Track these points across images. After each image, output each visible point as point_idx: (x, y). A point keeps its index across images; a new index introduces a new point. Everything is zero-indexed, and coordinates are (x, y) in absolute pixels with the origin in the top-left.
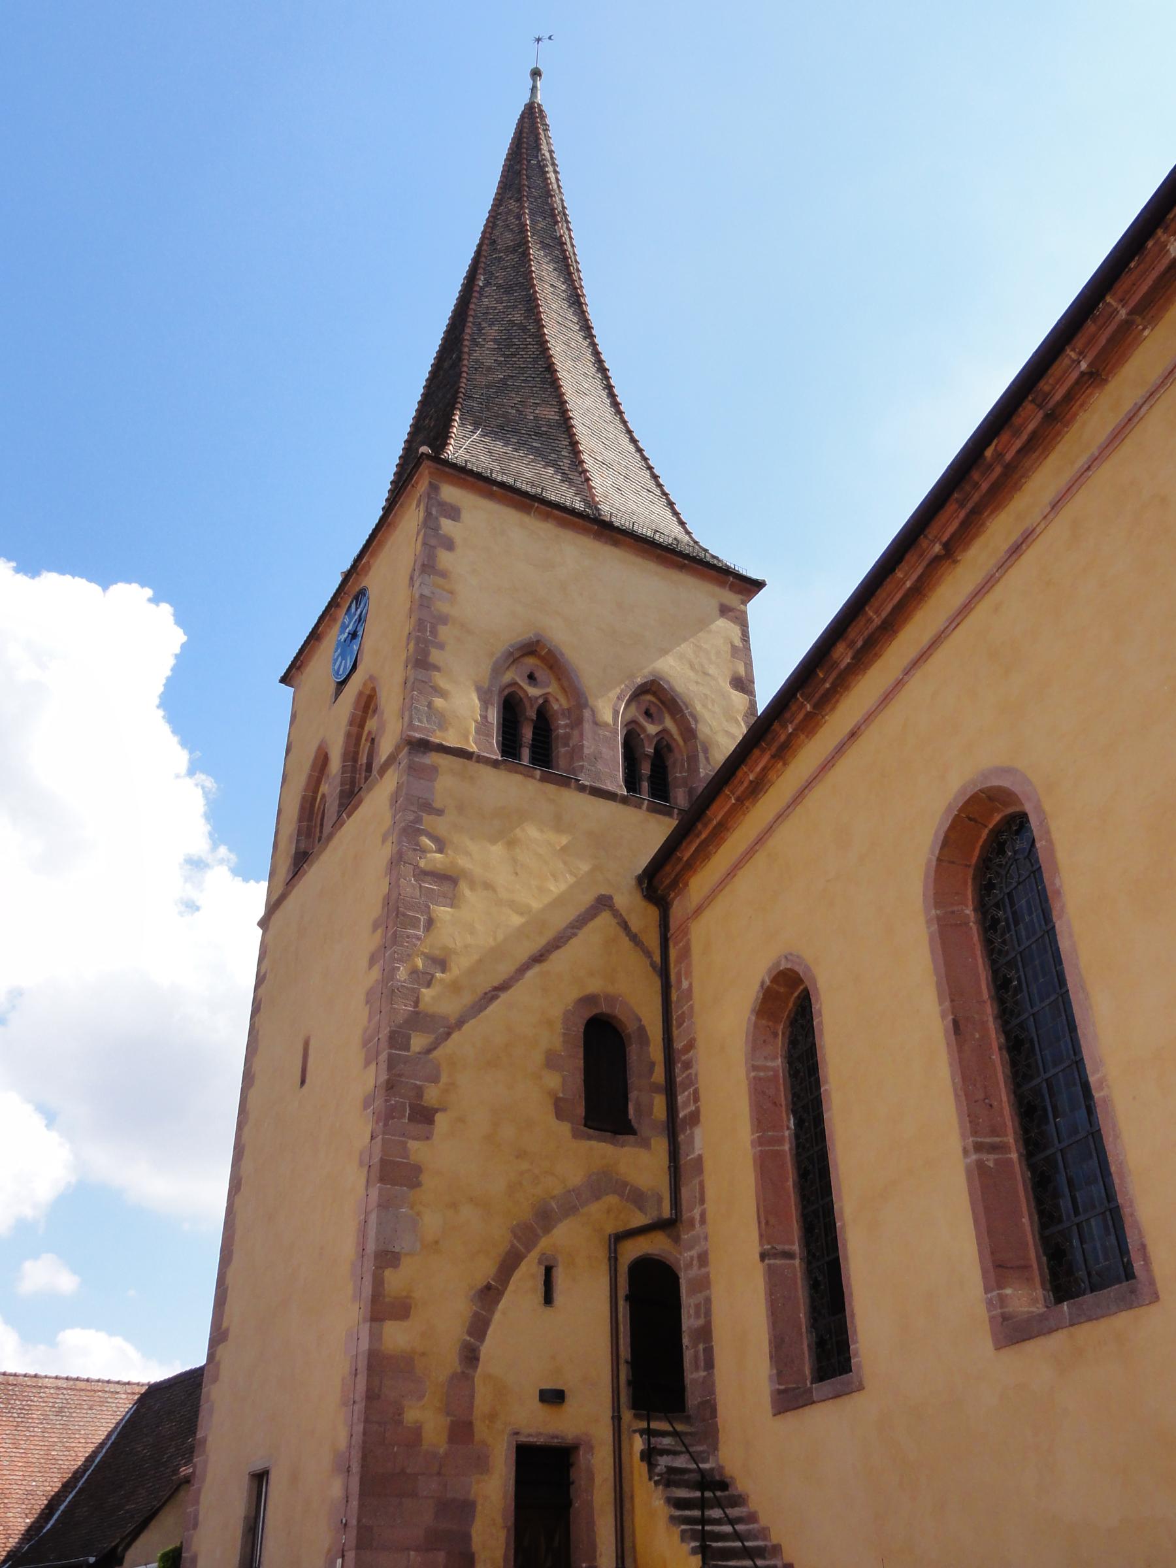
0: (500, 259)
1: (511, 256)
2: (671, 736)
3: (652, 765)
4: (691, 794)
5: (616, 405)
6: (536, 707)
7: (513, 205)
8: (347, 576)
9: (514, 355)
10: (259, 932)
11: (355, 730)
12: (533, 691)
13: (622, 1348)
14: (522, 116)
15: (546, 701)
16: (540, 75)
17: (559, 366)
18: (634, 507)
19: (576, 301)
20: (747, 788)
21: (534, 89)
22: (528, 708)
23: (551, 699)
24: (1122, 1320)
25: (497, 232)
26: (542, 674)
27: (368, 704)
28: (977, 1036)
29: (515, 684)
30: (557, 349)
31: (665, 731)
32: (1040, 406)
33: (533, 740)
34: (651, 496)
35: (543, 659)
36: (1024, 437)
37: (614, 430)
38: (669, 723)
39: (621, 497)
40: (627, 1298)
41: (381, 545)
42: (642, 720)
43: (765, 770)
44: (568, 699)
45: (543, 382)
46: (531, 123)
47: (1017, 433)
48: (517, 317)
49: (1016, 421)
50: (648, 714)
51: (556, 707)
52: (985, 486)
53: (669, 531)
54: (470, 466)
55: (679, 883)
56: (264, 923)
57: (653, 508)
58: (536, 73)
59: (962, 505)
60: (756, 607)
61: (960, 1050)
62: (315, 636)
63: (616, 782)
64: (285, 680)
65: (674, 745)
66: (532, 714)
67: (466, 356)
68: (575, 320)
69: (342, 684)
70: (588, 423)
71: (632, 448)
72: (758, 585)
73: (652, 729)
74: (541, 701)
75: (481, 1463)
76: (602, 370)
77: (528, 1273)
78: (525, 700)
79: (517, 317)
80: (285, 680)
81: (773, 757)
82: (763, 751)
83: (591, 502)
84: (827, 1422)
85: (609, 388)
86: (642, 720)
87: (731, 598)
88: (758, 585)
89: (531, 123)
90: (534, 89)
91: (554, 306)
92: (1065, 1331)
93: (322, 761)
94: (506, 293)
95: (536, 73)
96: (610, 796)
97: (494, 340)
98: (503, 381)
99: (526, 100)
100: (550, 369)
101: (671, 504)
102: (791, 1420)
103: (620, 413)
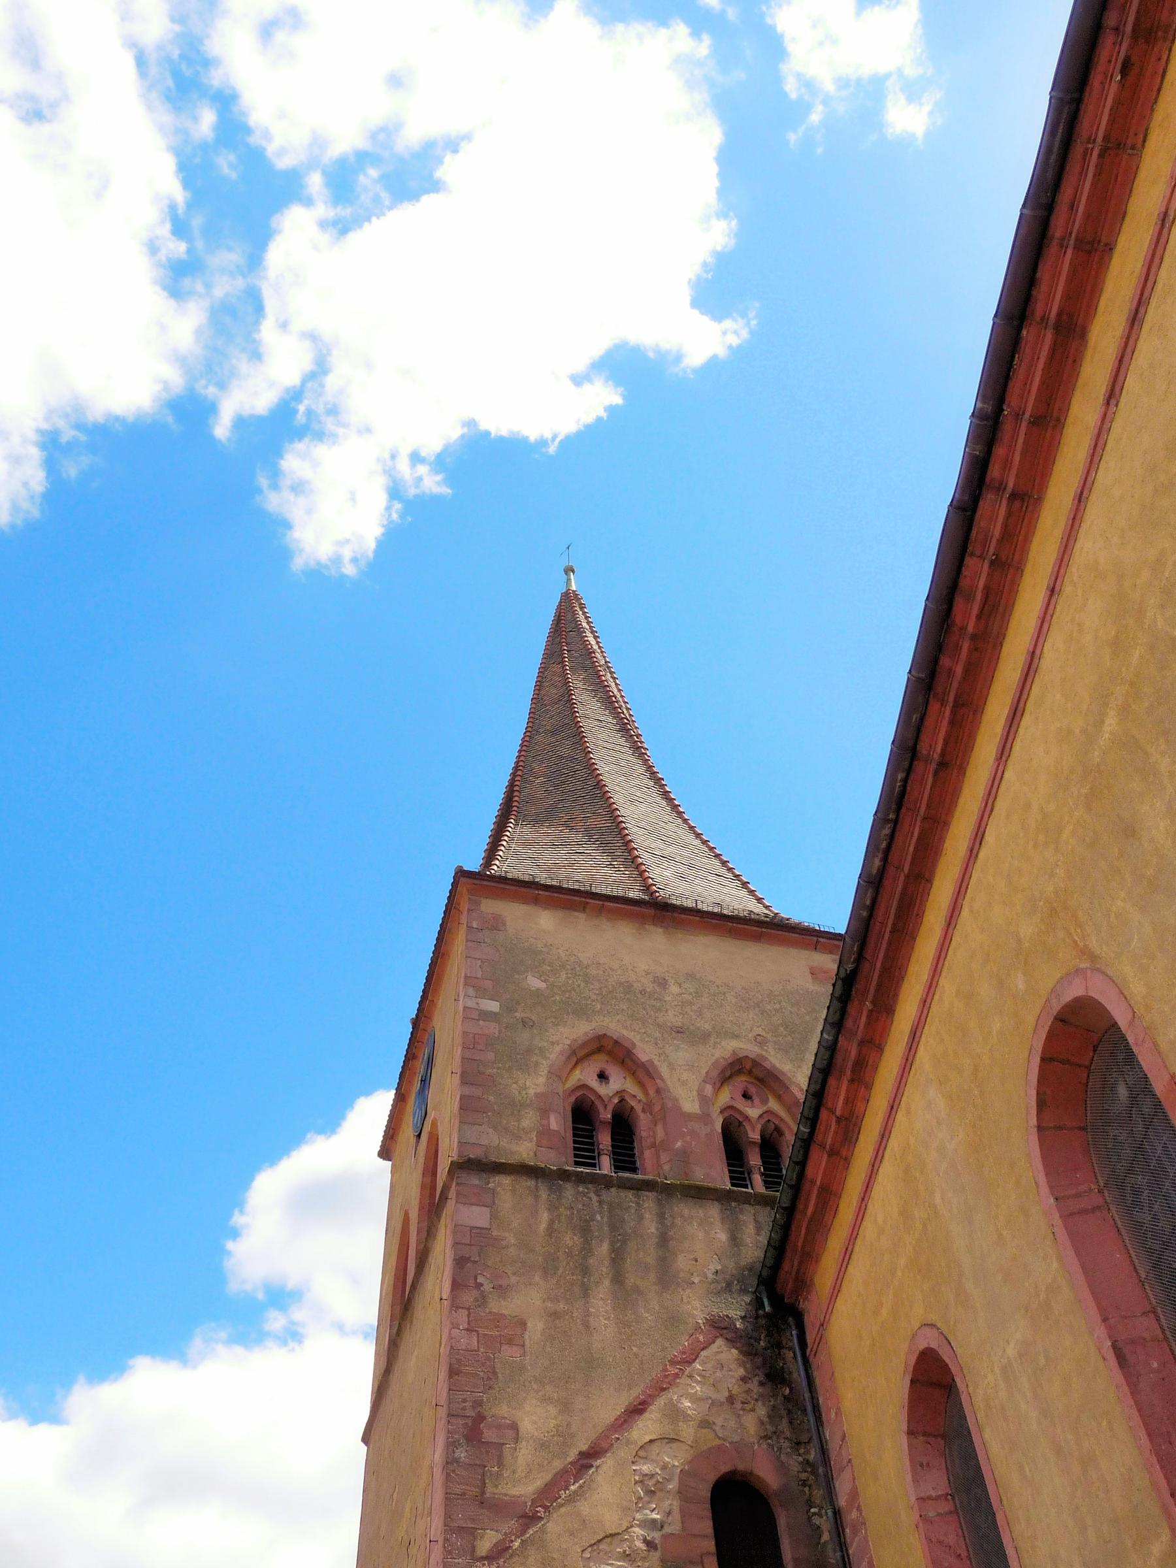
2: (777, 1116)
3: (762, 1157)
4: (789, 1167)
5: (675, 807)
6: (610, 1108)
7: (557, 668)
8: (416, 1023)
9: (563, 783)
10: (364, 1448)
12: (605, 1090)
15: (622, 1100)
17: (607, 780)
18: (700, 889)
19: (625, 728)
20: (836, 1132)
22: (601, 1109)
23: (627, 1098)
27: (434, 1139)
28: (1155, 1365)
29: (585, 1086)
30: (604, 768)
31: (769, 1112)
32: (982, 557)
33: (613, 1146)
34: (721, 879)
35: (610, 1053)
36: (979, 596)
37: (675, 828)
38: (773, 1104)
39: (679, 878)
41: (440, 978)
43: (850, 1101)
47: (970, 598)
49: (964, 583)
50: (746, 1096)
51: (633, 1103)
52: (959, 670)
53: (737, 902)
54: (510, 876)
56: (366, 1439)
57: (725, 890)
59: (943, 703)
61: (1134, 1392)
65: (783, 1127)
67: (516, 794)
68: (622, 741)
69: (419, 1136)
70: (642, 824)
71: (697, 842)
74: (616, 1101)
76: (658, 781)
78: (597, 1103)
81: (852, 1081)
82: (839, 1079)
83: (647, 888)
85: (666, 795)
96: (699, 1194)
100: (600, 785)
101: (745, 885)
103: (680, 814)
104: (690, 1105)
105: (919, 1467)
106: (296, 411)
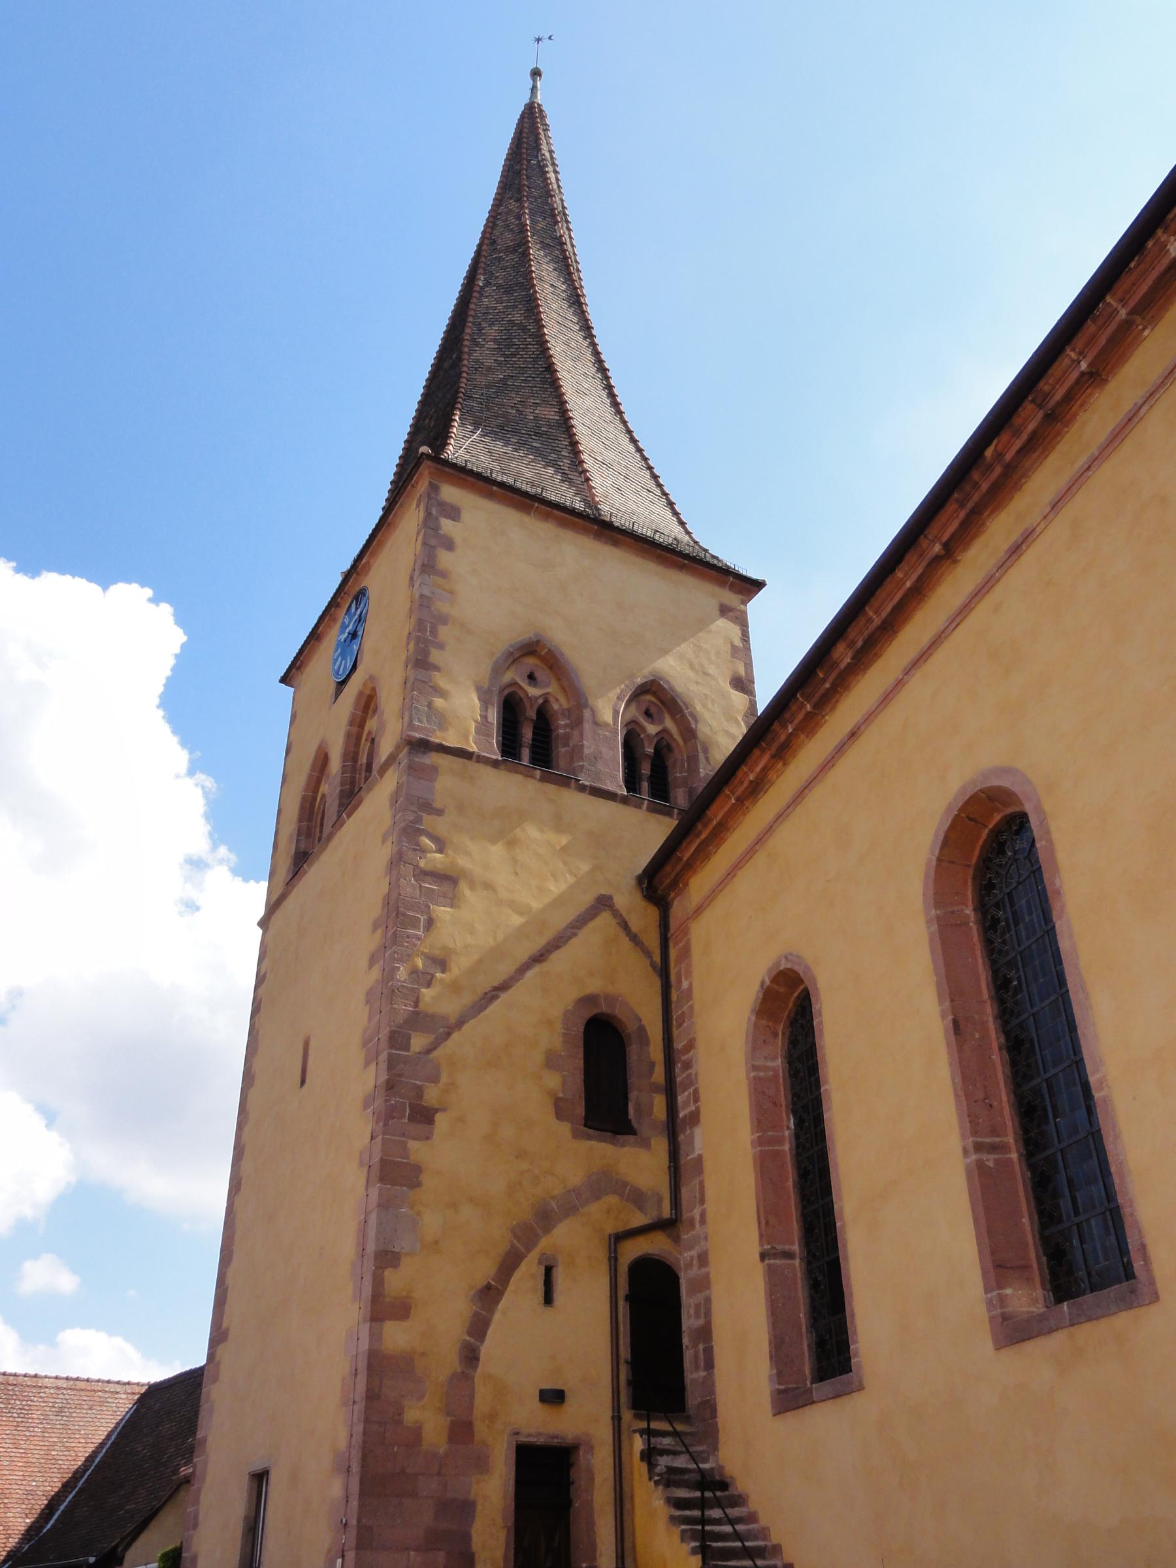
0: (500, 259)
1: (511, 256)
2: (671, 736)
3: (652, 765)
4: (691, 794)
5: (616, 405)
6: (536, 707)
7: (513, 205)
8: (347, 576)
9: (514, 355)
10: (259, 932)
11: (355, 730)
13: (622, 1348)
14: (522, 116)
15: (546, 701)
16: (540, 75)
17: (559, 366)
18: (634, 507)
19: (576, 301)
20: (747, 788)
21: (534, 89)
22: (528, 708)
24: (1122, 1320)
25: (497, 232)
26: (542, 674)
27: (368, 704)
29: (515, 684)
30: (557, 349)
31: (665, 731)
32: (1040, 406)
33: (533, 740)
34: (651, 496)
35: (543, 659)
36: (1024, 437)
37: (614, 430)
38: (669, 723)
39: (621, 497)
40: (627, 1298)
41: (381, 545)
42: (642, 720)
43: (765, 770)
44: (568, 699)
45: (543, 382)
46: (531, 123)
47: (1017, 433)
48: (517, 317)
49: (1016, 421)
50: (648, 714)
51: (556, 707)
52: (985, 486)
53: (669, 531)
54: (470, 466)
55: (679, 883)
56: (264, 923)
57: (653, 508)
58: (536, 73)
59: (962, 505)
60: (756, 607)
62: (315, 636)
63: (616, 782)
64: (285, 680)
65: (674, 745)
66: (532, 714)
67: (466, 356)
68: (575, 320)
69: (342, 684)
70: (588, 423)
71: (632, 448)
72: (758, 585)
73: (652, 729)
74: (541, 701)
75: (481, 1463)
76: (602, 370)
77: (528, 1273)
78: (525, 700)
79: (517, 317)
80: (285, 680)
81: (773, 757)
82: (763, 751)
83: (591, 502)
84: (827, 1422)
85: (609, 388)
86: (642, 720)
87: (731, 598)
88: (758, 585)
89: (531, 123)
90: (534, 89)
91: (554, 306)
92: (1065, 1331)
93: (322, 761)
94: (506, 293)
95: (536, 73)
97: (494, 340)
98: (503, 381)
99: (526, 100)
100: (550, 369)
101: (671, 504)
102: (791, 1420)
103: (620, 413)
104: (607, 716)
105: (756, 1043)
106: (853, 658)
